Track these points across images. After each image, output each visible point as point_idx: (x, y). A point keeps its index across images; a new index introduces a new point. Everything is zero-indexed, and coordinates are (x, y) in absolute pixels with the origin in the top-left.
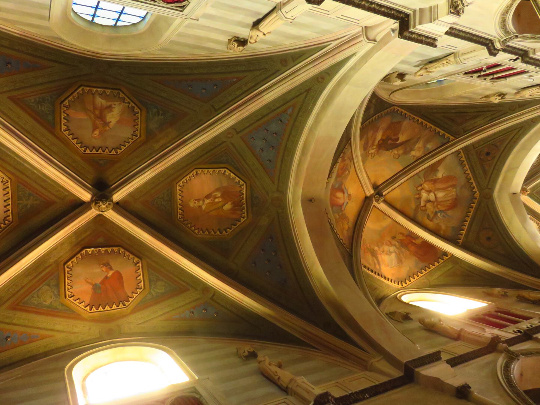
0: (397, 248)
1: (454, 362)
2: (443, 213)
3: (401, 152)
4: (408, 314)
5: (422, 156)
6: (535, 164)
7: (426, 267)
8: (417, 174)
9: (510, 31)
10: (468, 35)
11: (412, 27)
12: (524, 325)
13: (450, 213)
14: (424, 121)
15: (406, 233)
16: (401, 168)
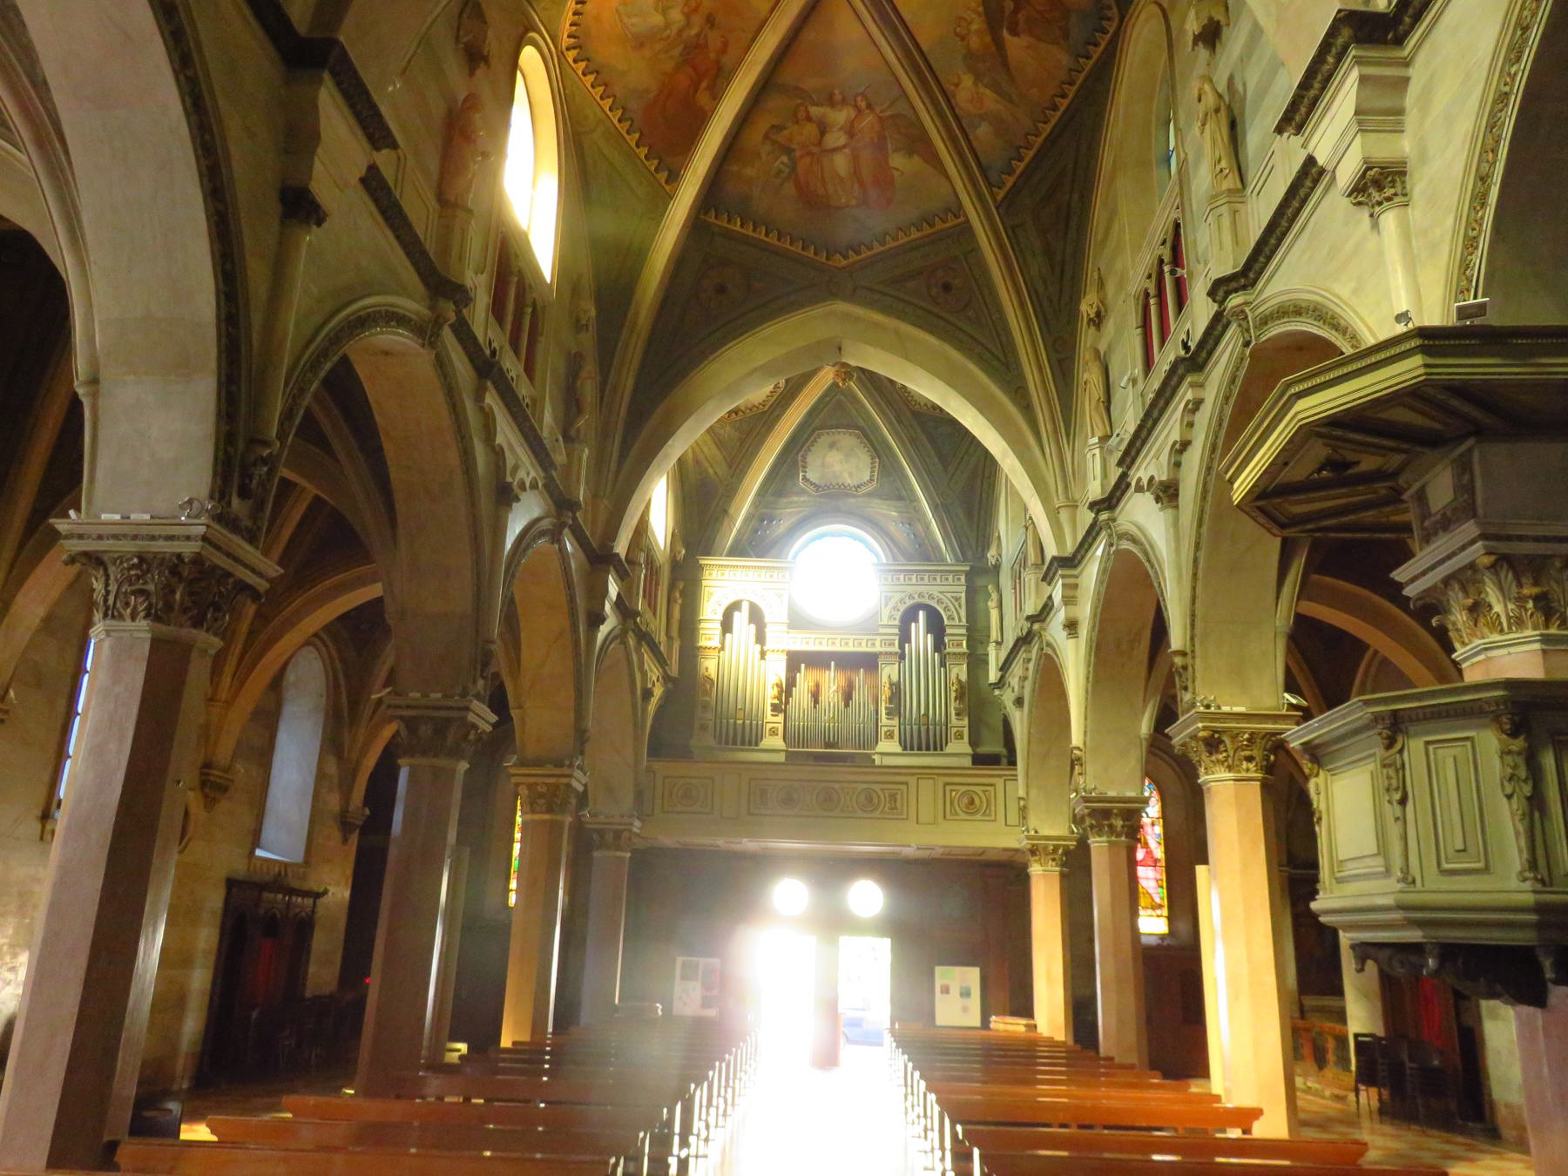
0: (680, 32)
1: (373, 183)
2: (787, 170)
3: (974, 42)
4: (485, 59)
5: (957, 111)
6: (910, 398)
7: (632, 121)
8: (904, 93)
9: (1265, 328)
10: (1284, 224)
11: (1361, 53)
12: (512, 366)
13: (790, 189)
14: (1059, 113)
15: (727, 60)
16: (925, 48)
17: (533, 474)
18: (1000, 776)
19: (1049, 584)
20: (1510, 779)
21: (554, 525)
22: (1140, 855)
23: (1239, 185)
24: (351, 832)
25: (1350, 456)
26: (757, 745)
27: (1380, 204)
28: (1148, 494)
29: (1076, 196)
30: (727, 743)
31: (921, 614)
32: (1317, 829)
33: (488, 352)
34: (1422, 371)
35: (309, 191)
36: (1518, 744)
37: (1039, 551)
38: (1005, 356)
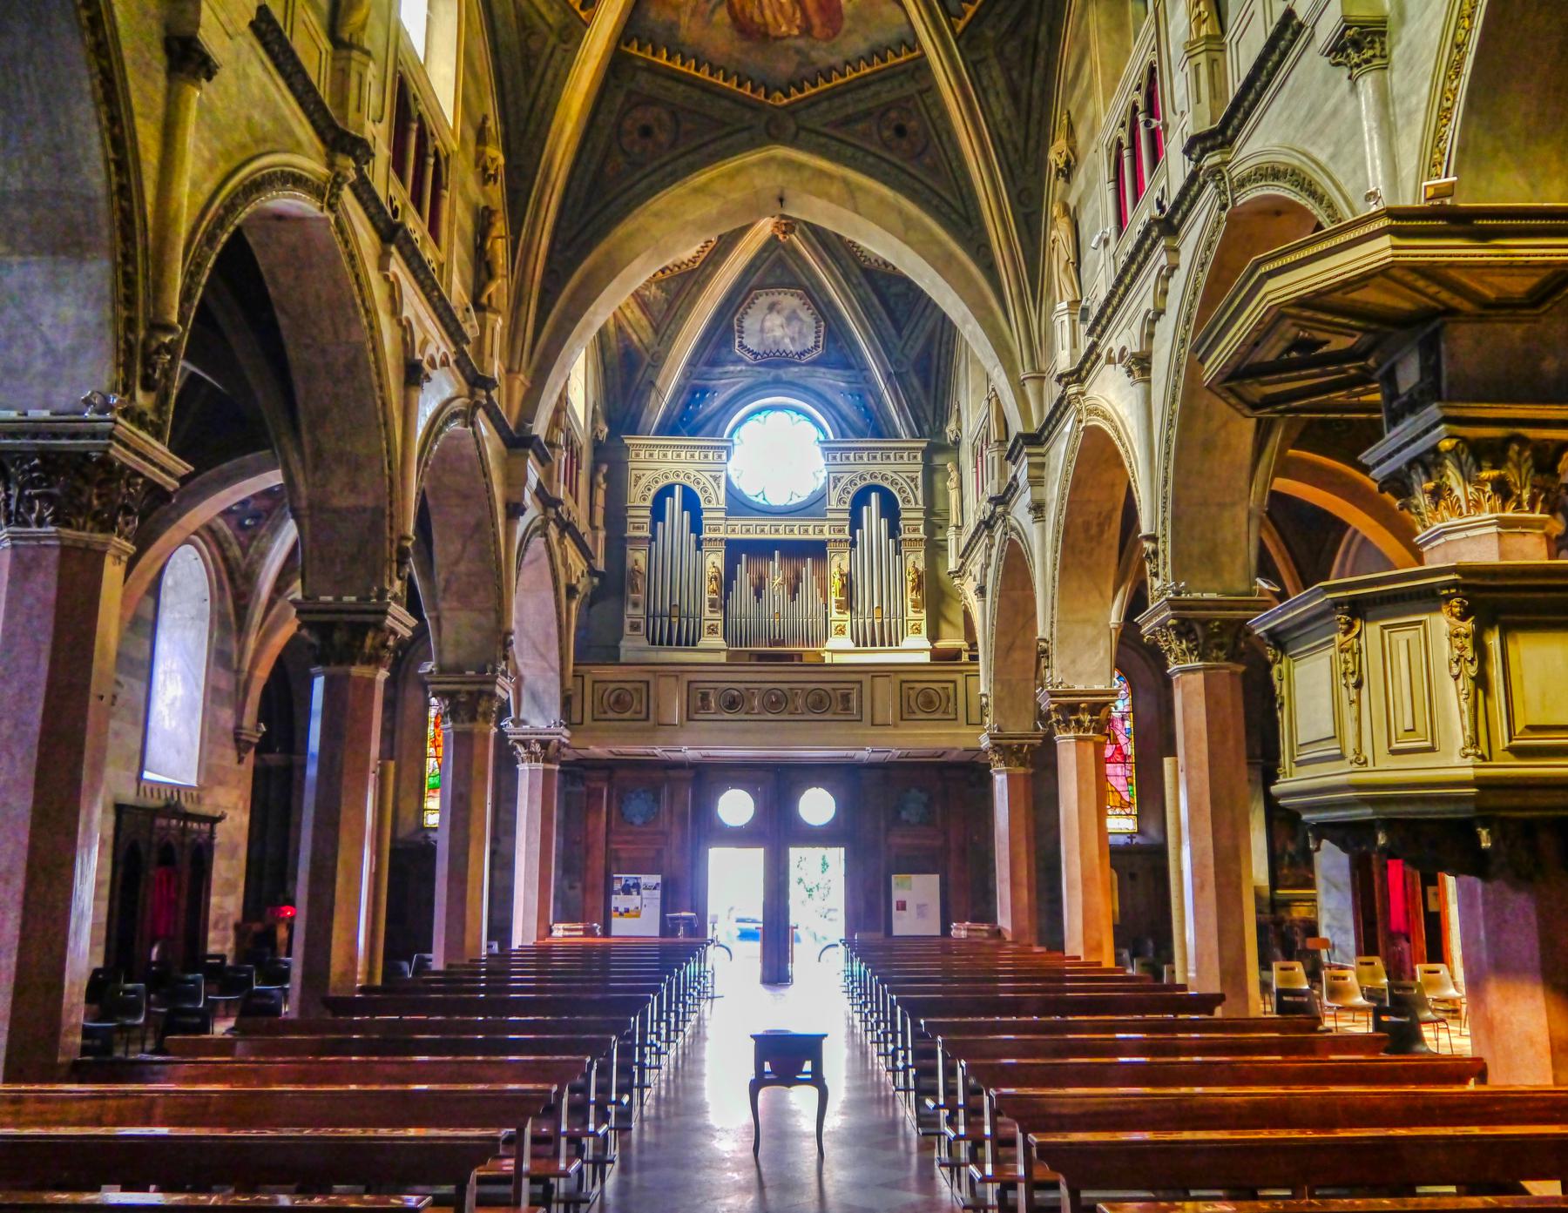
12: (415, 225)
17: (443, 349)
18: (960, 672)
19: (1014, 463)
20: (1457, 662)
21: (468, 406)
22: (1109, 751)
23: (1218, 32)
24: (247, 751)
25: (1321, 336)
26: (694, 644)
27: (1358, 65)
28: (1119, 366)
29: (1044, 28)
30: (882, 644)
31: (874, 497)
32: (1279, 714)
33: (389, 211)
34: (1390, 252)
35: (197, 41)
36: (1468, 626)
37: (1002, 426)
38: (965, 207)
